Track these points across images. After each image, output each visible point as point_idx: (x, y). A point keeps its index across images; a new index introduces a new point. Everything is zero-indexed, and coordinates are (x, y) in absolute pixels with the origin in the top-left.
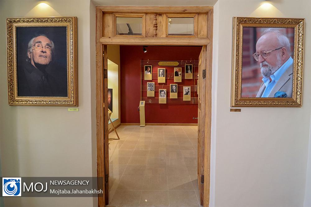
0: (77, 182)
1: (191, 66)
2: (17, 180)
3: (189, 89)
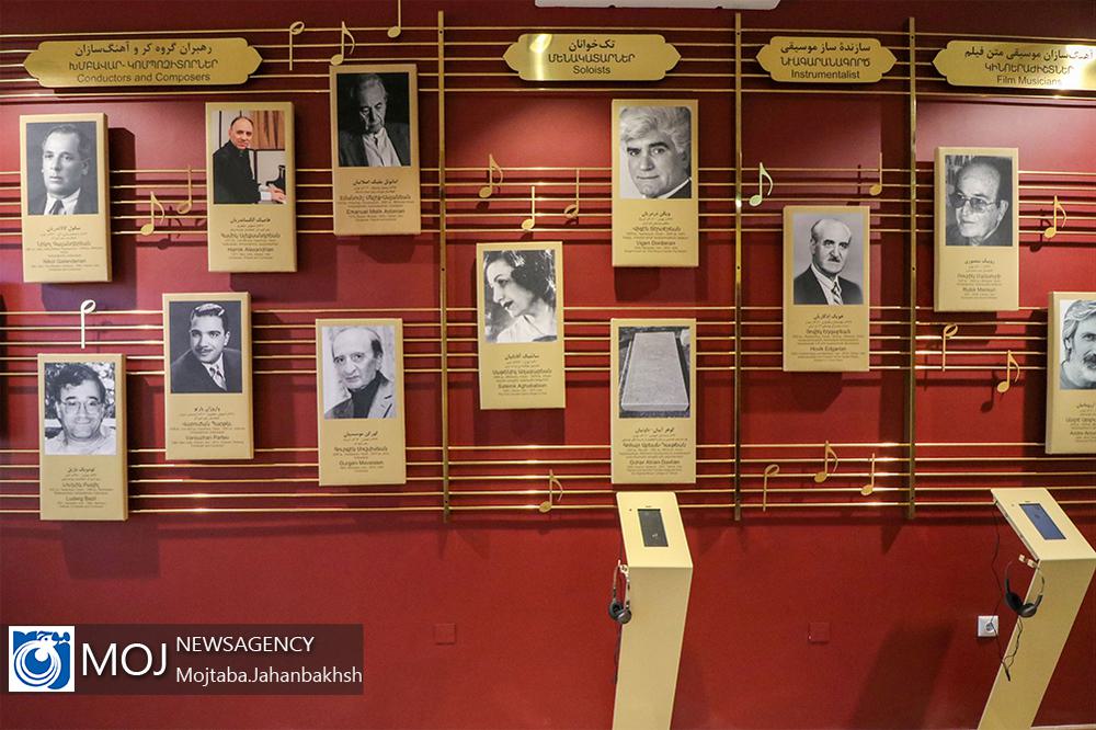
0: (272, 641)
1: (395, 85)
2: (61, 635)
3: (376, 347)
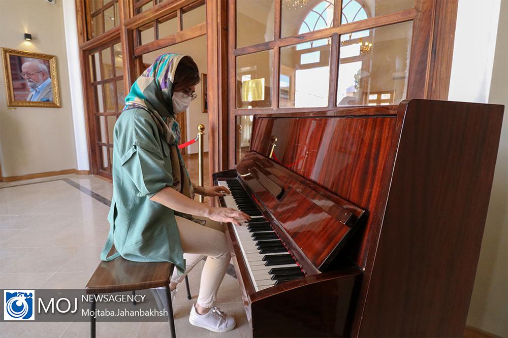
2: (28, 294)
